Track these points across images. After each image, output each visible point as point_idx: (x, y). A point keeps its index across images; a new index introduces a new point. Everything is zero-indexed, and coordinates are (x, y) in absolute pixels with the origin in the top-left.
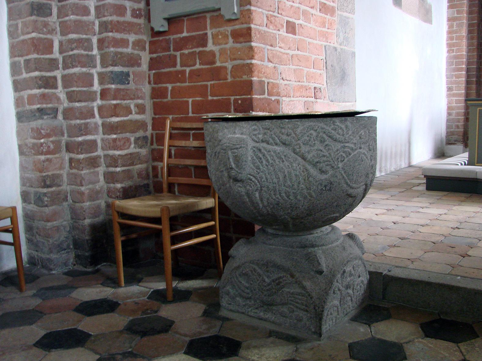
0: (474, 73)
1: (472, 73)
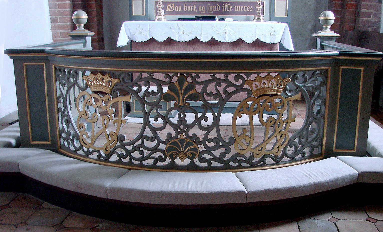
0: (79, 3)
1: (78, 3)
